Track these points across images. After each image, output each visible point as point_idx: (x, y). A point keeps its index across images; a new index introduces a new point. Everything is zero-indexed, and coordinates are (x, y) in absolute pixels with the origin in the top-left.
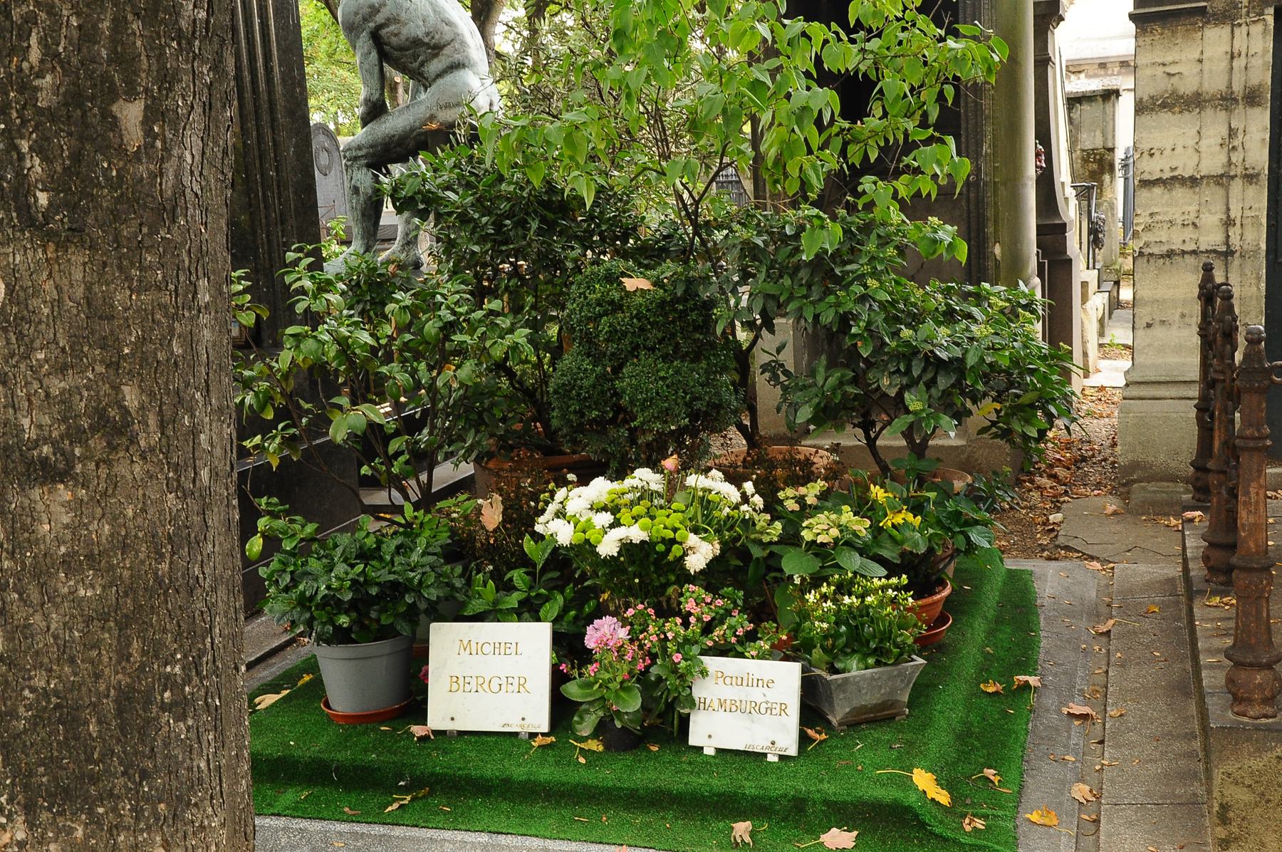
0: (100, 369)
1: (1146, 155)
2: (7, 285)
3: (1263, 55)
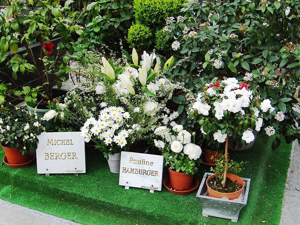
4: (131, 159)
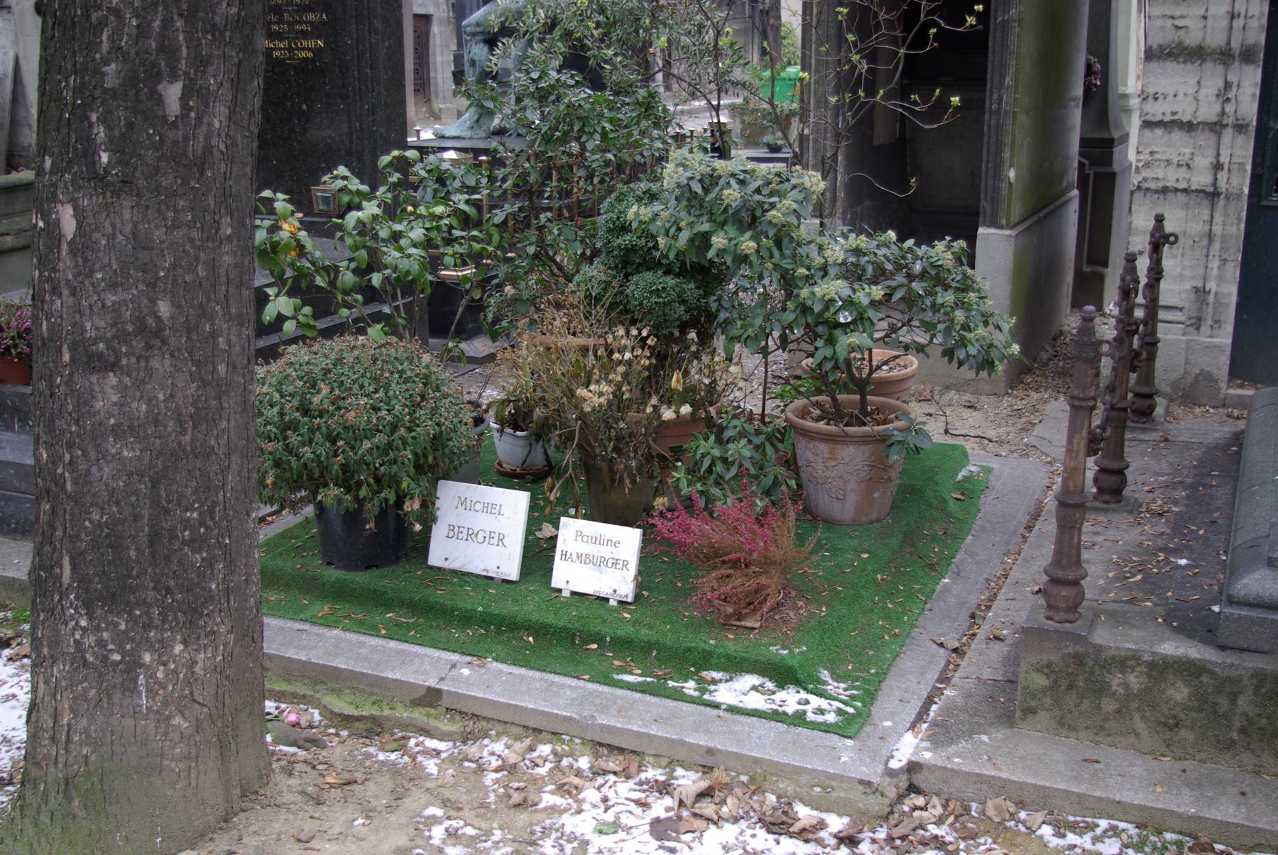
0: (142, 287)
1: (1150, 99)
2: (78, 222)
3: (1259, 18)
4: (579, 534)
